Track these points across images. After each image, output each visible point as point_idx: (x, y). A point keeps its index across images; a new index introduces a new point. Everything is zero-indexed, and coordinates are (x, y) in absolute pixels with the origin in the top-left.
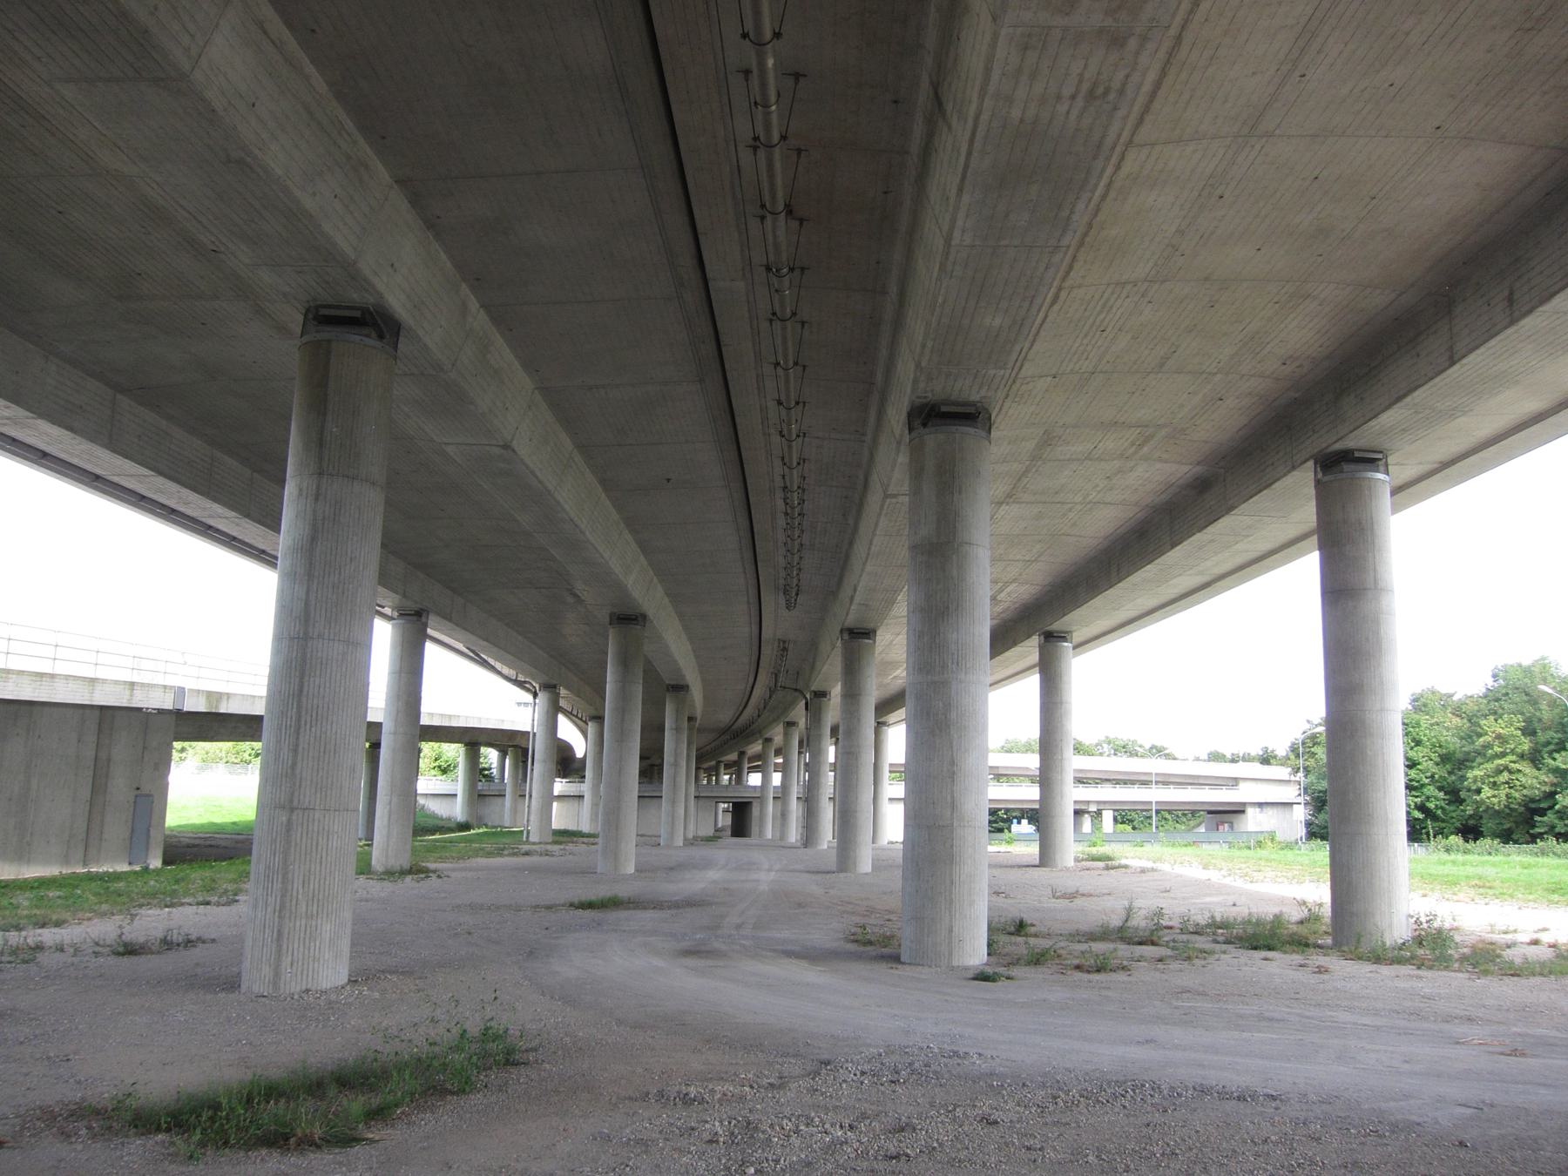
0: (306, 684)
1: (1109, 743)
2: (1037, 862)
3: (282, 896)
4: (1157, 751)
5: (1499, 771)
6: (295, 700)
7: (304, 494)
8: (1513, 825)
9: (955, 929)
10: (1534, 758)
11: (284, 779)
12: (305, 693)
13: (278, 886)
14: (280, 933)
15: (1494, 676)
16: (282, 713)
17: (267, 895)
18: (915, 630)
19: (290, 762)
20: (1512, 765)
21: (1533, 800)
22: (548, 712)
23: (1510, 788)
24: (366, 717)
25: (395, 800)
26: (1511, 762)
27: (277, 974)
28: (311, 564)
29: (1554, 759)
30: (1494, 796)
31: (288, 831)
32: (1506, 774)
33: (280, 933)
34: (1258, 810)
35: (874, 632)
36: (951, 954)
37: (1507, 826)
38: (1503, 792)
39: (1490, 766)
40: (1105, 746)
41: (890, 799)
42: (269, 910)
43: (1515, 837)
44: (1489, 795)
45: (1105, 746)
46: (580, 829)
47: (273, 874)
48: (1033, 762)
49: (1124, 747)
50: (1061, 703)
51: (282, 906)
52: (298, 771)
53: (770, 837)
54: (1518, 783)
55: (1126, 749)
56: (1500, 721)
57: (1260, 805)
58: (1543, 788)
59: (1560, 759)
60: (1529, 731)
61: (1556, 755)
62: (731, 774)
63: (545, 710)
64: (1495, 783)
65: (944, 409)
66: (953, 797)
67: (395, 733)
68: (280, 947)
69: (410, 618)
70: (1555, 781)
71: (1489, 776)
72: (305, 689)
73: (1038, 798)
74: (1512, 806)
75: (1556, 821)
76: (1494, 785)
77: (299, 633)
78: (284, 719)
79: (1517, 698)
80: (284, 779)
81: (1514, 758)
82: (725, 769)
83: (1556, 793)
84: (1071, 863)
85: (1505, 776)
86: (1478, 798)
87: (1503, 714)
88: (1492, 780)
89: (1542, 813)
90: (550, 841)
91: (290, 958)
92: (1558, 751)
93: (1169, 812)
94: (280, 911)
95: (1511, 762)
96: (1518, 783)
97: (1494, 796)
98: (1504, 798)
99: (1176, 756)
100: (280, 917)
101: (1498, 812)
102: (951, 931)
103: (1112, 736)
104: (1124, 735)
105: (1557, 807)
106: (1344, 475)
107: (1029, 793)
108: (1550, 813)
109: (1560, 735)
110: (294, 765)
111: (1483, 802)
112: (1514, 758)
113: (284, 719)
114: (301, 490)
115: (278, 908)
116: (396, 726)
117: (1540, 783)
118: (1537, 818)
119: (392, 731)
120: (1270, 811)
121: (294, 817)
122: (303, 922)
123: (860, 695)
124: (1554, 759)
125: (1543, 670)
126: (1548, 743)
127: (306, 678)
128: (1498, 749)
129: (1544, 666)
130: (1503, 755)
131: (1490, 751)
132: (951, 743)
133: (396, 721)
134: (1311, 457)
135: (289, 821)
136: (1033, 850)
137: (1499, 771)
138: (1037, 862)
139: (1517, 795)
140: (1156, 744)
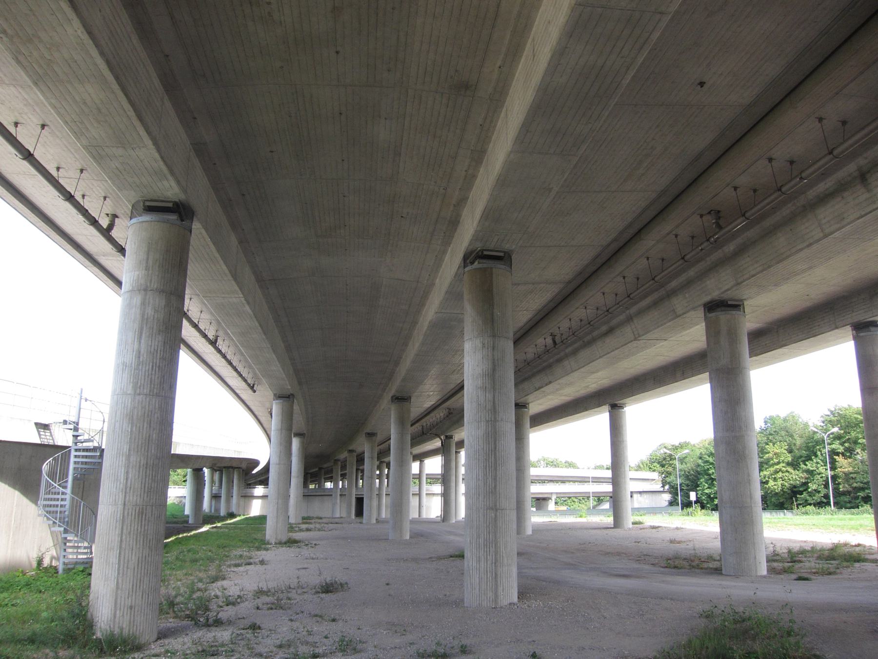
0: (497, 445)
1: (544, 460)
2: (613, 526)
3: (495, 555)
4: (570, 465)
5: (776, 472)
6: (493, 453)
7: (486, 346)
8: (784, 500)
9: (757, 557)
10: (794, 464)
11: (491, 495)
12: (497, 449)
13: (492, 550)
14: (496, 574)
15: (766, 422)
16: (486, 459)
17: (487, 555)
18: (722, 410)
19: (493, 486)
20: (784, 468)
21: (795, 487)
22: (299, 449)
23: (783, 480)
24: (171, 451)
25: (280, 501)
26: (783, 467)
27: (496, 596)
28: (494, 382)
29: (806, 465)
30: (775, 485)
31: (496, 521)
32: (780, 473)
33: (496, 574)
34: (639, 495)
35: (410, 398)
36: (756, 570)
37: (781, 501)
38: (780, 482)
39: (772, 469)
40: (542, 462)
41: (413, 494)
42: (489, 562)
43: (786, 506)
44: (773, 484)
45: (542, 462)
46: (308, 515)
47: (489, 544)
48: (609, 474)
49: (552, 462)
50: (623, 441)
51: (496, 560)
52: (497, 490)
53: (384, 517)
54: (787, 478)
55: (553, 464)
56: (775, 446)
57: (640, 492)
58: (801, 480)
59: (809, 465)
60: (790, 451)
61: (807, 463)
62: (316, 484)
63: (298, 448)
64: (775, 478)
65: (730, 303)
66: (750, 492)
67: (279, 464)
68: (496, 581)
69: (285, 399)
70: (807, 476)
71: (772, 475)
72: (497, 448)
73: (611, 490)
74: (784, 490)
75: (808, 497)
76: (775, 479)
77: (491, 418)
78: (488, 463)
79: (783, 433)
80: (491, 495)
81: (784, 465)
82: (311, 478)
83: (808, 483)
84: (631, 526)
85: (780, 475)
86: (767, 486)
87: (776, 442)
88: (773, 476)
89: (801, 493)
90: (301, 522)
91: (502, 588)
92: (807, 461)
93: (576, 497)
94: (495, 563)
95: (783, 467)
96: (787, 478)
97: (775, 485)
98: (780, 486)
99: (579, 467)
100: (495, 566)
101: (776, 494)
102: (755, 558)
103: (546, 456)
104: (551, 456)
105: (810, 490)
106: (871, 333)
107: (608, 488)
108: (805, 494)
109: (807, 453)
110: (495, 486)
111: (769, 488)
112: (784, 465)
113: (488, 463)
114: (484, 344)
115: (494, 561)
116: (279, 460)
117: (799, 478)
118: (798, 496)
119: (278, 462)
120: (645, 496)
121: (498, 514)
122: (506, 568)
123: (523, 438)
124: (806, 465)
125: (792, 418)
126: (801, 457)
127: (497, 442)
128: (776, 461)
129: (793, 417)
130: (779, 463)
131: (772, 462)
132: (747, 466)
133: (280, 457)
134: (851, 324)
135: (496, 516)
136: (609, 520)
137: (776, 472)
138: (613, 526)
139: (786, 484)
140: (568, 460)
